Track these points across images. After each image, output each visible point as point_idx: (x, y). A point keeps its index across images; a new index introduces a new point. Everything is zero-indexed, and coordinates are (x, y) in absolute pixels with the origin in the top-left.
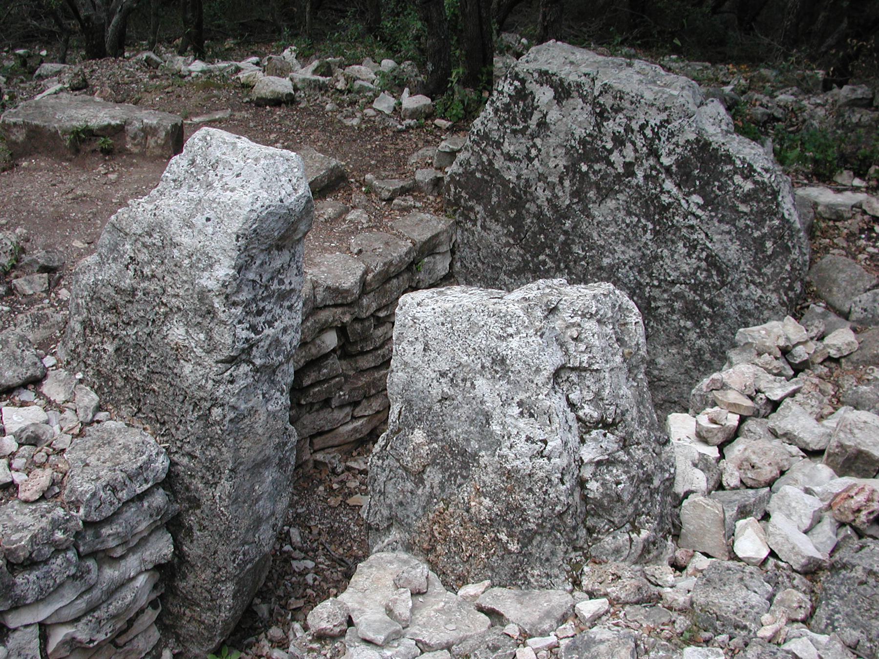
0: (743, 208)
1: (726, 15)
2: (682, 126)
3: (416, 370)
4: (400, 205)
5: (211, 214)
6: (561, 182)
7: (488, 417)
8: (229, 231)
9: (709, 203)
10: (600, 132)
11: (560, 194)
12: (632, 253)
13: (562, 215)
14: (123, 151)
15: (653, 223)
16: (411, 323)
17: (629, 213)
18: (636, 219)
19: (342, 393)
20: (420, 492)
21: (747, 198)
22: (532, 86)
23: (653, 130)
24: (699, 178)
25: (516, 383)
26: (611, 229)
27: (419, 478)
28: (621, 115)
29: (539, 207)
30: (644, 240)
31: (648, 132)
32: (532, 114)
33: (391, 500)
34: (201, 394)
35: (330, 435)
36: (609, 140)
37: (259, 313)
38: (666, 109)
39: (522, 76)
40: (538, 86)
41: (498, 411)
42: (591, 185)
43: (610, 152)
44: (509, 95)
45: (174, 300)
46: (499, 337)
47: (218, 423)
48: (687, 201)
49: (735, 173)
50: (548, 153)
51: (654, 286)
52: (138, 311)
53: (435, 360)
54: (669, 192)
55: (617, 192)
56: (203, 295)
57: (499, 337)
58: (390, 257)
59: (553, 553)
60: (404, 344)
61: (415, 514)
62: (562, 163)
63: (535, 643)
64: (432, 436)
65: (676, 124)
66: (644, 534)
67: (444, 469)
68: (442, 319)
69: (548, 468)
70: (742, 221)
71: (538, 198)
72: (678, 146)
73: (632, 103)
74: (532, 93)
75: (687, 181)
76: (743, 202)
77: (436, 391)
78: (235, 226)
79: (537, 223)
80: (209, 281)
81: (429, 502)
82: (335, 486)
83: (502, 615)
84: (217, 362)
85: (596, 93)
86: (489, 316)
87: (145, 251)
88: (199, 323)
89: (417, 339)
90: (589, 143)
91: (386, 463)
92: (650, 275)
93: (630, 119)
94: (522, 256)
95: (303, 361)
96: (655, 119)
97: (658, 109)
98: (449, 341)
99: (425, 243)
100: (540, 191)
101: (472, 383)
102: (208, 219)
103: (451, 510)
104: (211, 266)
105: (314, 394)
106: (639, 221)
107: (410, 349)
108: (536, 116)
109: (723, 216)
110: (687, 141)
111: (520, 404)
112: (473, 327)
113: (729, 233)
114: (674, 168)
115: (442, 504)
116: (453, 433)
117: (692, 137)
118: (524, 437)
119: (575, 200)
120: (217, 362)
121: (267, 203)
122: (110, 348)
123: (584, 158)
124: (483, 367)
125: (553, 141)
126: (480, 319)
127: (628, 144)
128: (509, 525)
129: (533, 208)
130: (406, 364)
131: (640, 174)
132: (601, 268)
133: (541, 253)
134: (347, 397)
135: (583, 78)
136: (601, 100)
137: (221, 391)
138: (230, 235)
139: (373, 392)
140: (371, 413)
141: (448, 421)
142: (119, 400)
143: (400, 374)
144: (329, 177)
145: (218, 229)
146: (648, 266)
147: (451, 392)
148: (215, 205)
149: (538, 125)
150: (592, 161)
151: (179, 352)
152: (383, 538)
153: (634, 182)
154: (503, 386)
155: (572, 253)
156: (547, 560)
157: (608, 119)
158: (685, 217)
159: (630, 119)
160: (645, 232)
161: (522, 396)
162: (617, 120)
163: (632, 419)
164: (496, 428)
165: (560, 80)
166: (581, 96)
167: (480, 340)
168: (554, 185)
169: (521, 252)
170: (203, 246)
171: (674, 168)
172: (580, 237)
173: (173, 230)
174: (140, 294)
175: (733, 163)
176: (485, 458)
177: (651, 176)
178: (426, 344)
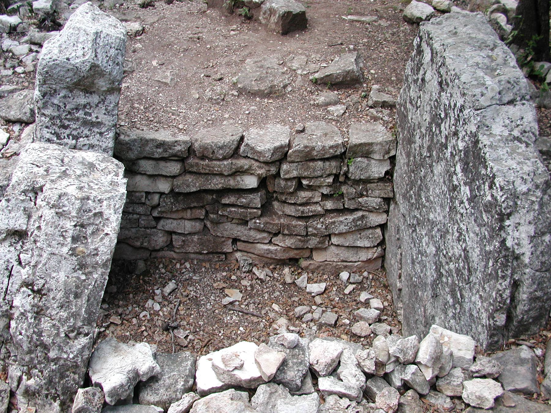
4: (372, 114)
14: (257, 20)
19: (258, 221)
35: (250, 245)
37: (65, 127)
58: (314, 144)
66: (31, 382)
82: (234, 277)
95: (220, 186)
99: (355, 145)
105: (231, 211)
121: (55, 57)
134: (262, 226)
139: (286, 232)
140: (283, 245)
144: (345, 77)
163: (54, 299)
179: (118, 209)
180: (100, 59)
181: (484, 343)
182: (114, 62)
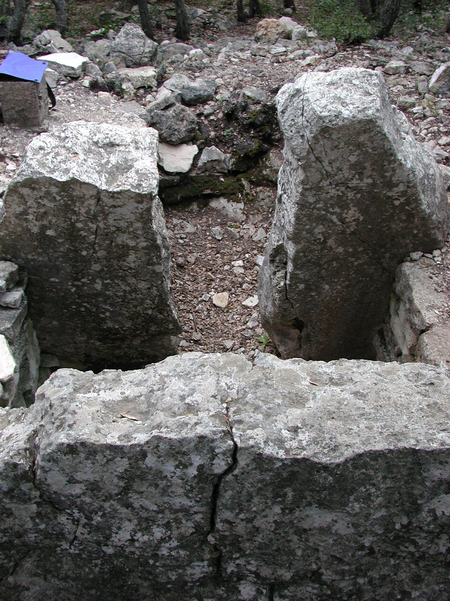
179: (23, 175)
180: (285, 118)
181: (322, 48)
182: (299, 132)
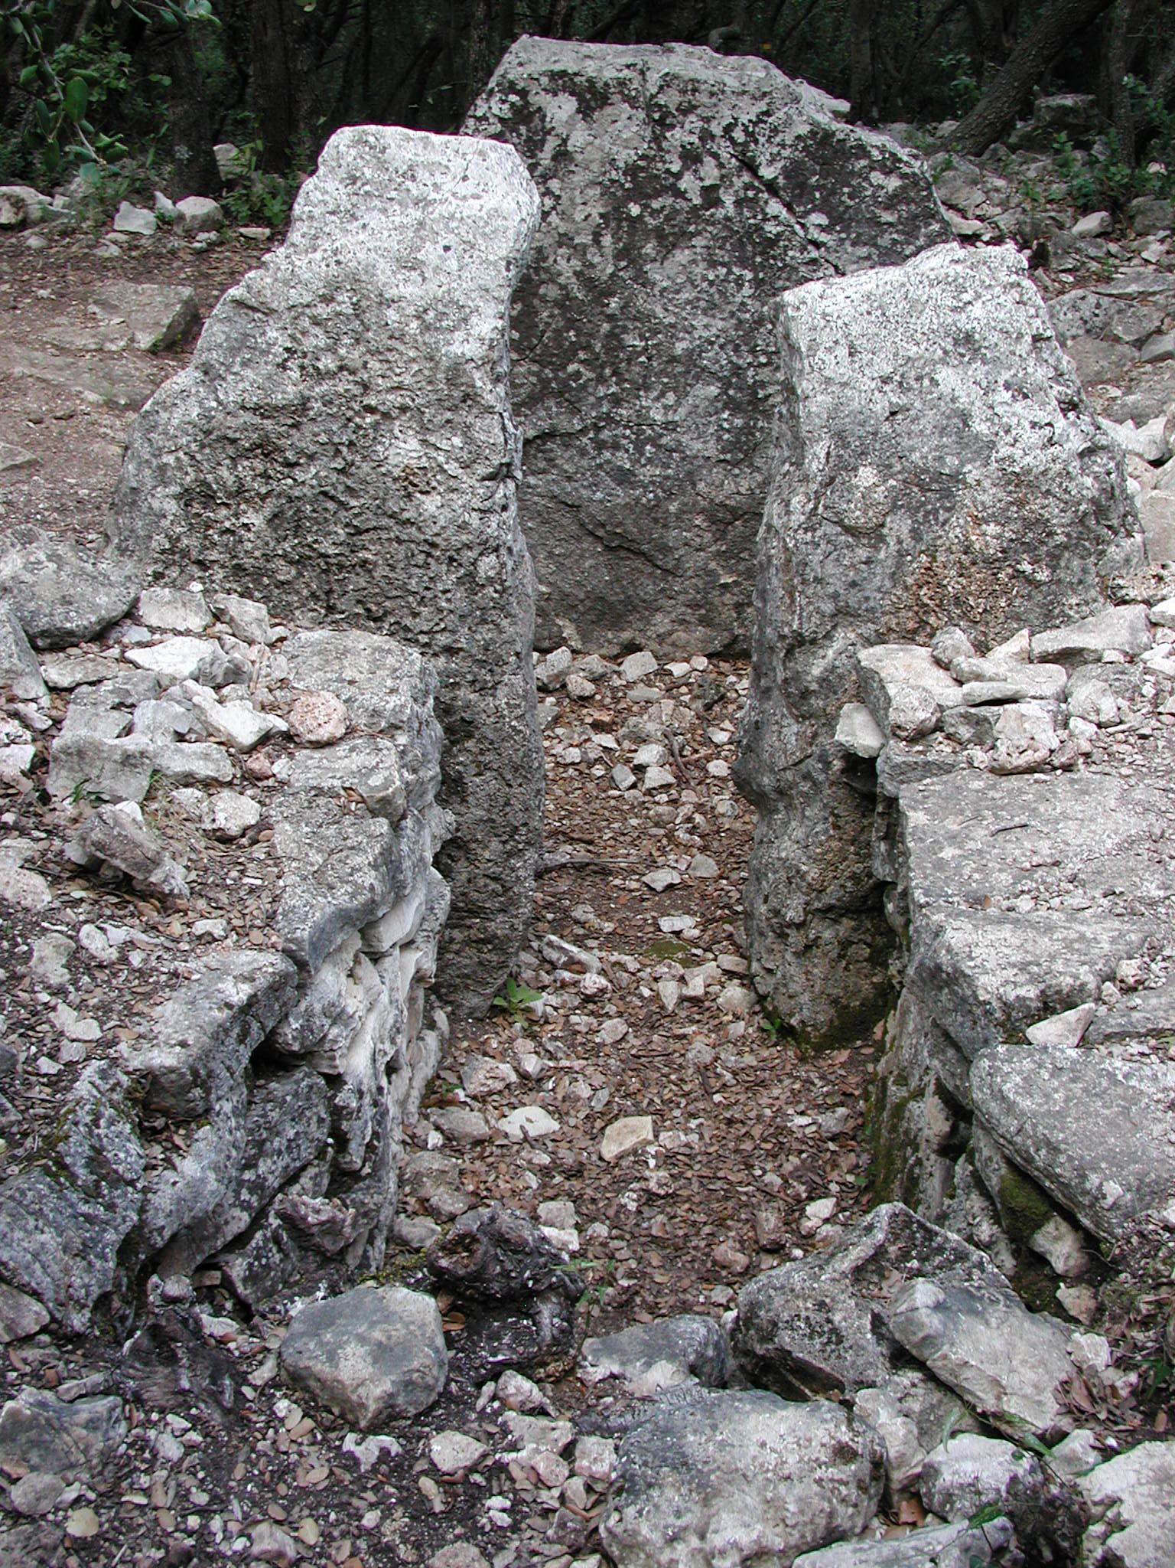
0: (887, 217)
1: (360, 89)
2: (789, 116)
3: (845, 384)
5: (451, 240)
6: (597, 237)
7: (965, 417)
8: (491, 258)
9: (838, 220)
10: (660, 149)
11: (596, 260)
12: (720, 324)
13: (599, 291)
15: (754, 269)
16: (823, 323)
17: (713, 264)
18: (724, 270)
20: (882, 555)
21: (892, 202)
22: (539, 99)
23: (745, 130)
24: (818, 188)
25: (995, 360)
26: (685, 295)
27: (875, 535)
28: (692, 118)
29: (563, 287)
30: (738, 299)
31: (739, 135)
32: (543, 142)
33: (836, 585)
34: (464, 538)
36: (675, 158)
38: (765, 94)
39: (521, 85)
40: (549, 97)
41: (978, 404)
42: (647, 234)
43: (678, 176)
44: (501, 120)
45: (391, 397)
46: (954, 309)
47: (490, 581)
48: (803, 226)
49: (873, 169)
50: (572, 200)
51: (761, 365)
52: (316, 435)
53: (870, 363)
54: (776, 217)
55: (693, 235)
56: (456, 372)
57: (954, 309)
59: (1085, 571)
60: (820, 354)
61: (879, 590)
62: (596, 210)
63: (69, 1390)
64: (885, 470)
65: (780, 114)
67: (913, 511)
68: (865, 306)
69: (1064, 456)
70: (887, 236)
71: (560, 274)
72: (783, 146)
73: (712, 94)
74: (540, 109)
75: (801, 195)
76: (888, 208)
77: (881, 407)
78: (503, 248)
79: (562, 315)
80: (465, 345)
81: (899, 565)
83: (1082, 650)
84: (484, 479)
85: (654, 90)
86: (932, 286)
87: (317, 330)
88: (448, 421)
89: (836, 342)
90: (642, 169)
91: (819, 533)
92: (753, 351)
93: (707, 120)
94: (536, 374)
96: (748, 112)
97: (754, 98)
98: (884, 332)
100: (562, 262)
101: (932, 380)
102: (447, 249)
103: (941, 558)
104: (465, 320)
106: (730, 272)
107: (829, 359)
108: (551, 144)
109: (859, 235)
110: (798, 137)
111: (1007, 386)
112: (915, 307)
113: (868, 258)
114: (781, 181)
115: (924, 558)
116: (915, 456)
117: (804, 130)
118: (1028, 426)
119: (623, 264)
120: (484, 479)
122: (256, 519)
123: (638, 193)
124: (946, 352)
125: (579, 178)
126: (922, 293)
127: (708, 159)
128: (1029, 548)
129: (551, 291)
130: (828, 381)
131: (728, 200)
132: (673, 359)
133: (570, 361)
135: (626, 71)
136: (662, 100)
137: (494, 525)
138: (495, 264)
141: (906, 442)
142: (289, 604)
143: (820, 398)
145: (467, 260)
146: (748, 337)
147: (903, 401)
148: (454, 224)
149: (554, 158)
150: (650, 197)
151: (411, 483)
152: (821, 652)
153: (720, 213)
154: (978, 370)
155: (623, 348)
156: (1080, 582)
157: (672, 127)
158: (803, 249)
159: (707, 120)
160: (740, 286)
161: (1006, 375)
162: (687, 126)
164: (980, 427)
165: (590, 80)
166: (627, 99)
167: (927, 319)
168: (585, 246)
169: (535, 368)
170: (449, 291)
171: (781, 181)
172: (635, 319)
173: (383, 279)
174: (317, 405)
175: (868, 155)
176: (973, 472)
177: (746, 199)
178: (851, 346)
